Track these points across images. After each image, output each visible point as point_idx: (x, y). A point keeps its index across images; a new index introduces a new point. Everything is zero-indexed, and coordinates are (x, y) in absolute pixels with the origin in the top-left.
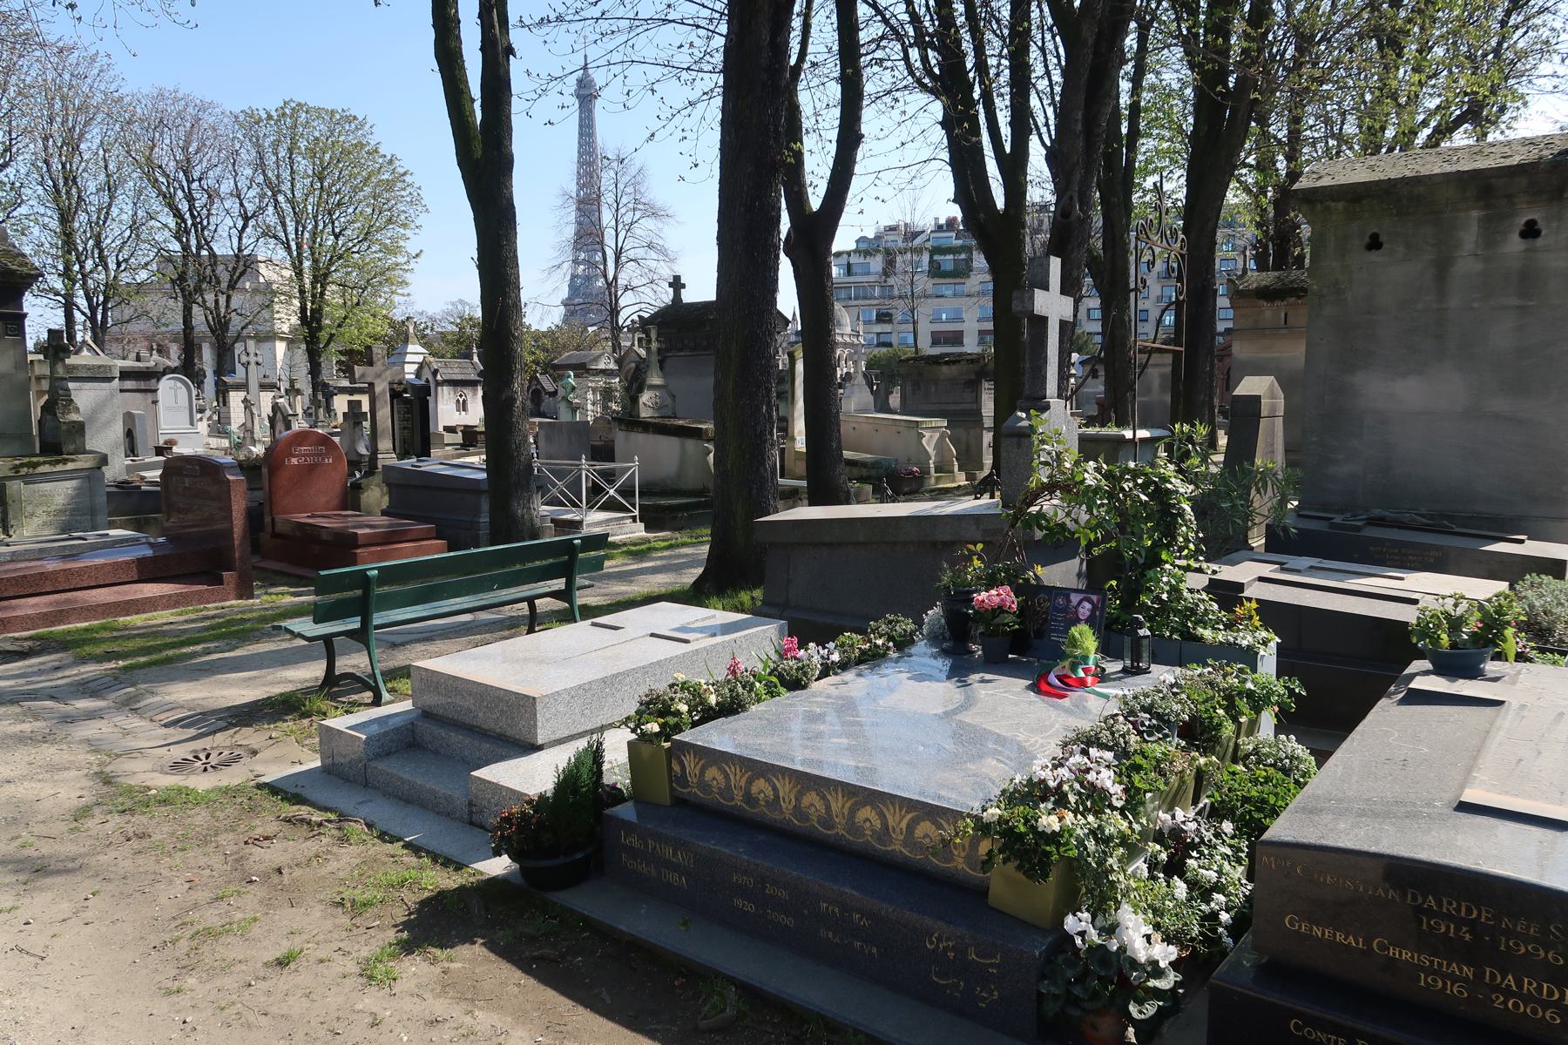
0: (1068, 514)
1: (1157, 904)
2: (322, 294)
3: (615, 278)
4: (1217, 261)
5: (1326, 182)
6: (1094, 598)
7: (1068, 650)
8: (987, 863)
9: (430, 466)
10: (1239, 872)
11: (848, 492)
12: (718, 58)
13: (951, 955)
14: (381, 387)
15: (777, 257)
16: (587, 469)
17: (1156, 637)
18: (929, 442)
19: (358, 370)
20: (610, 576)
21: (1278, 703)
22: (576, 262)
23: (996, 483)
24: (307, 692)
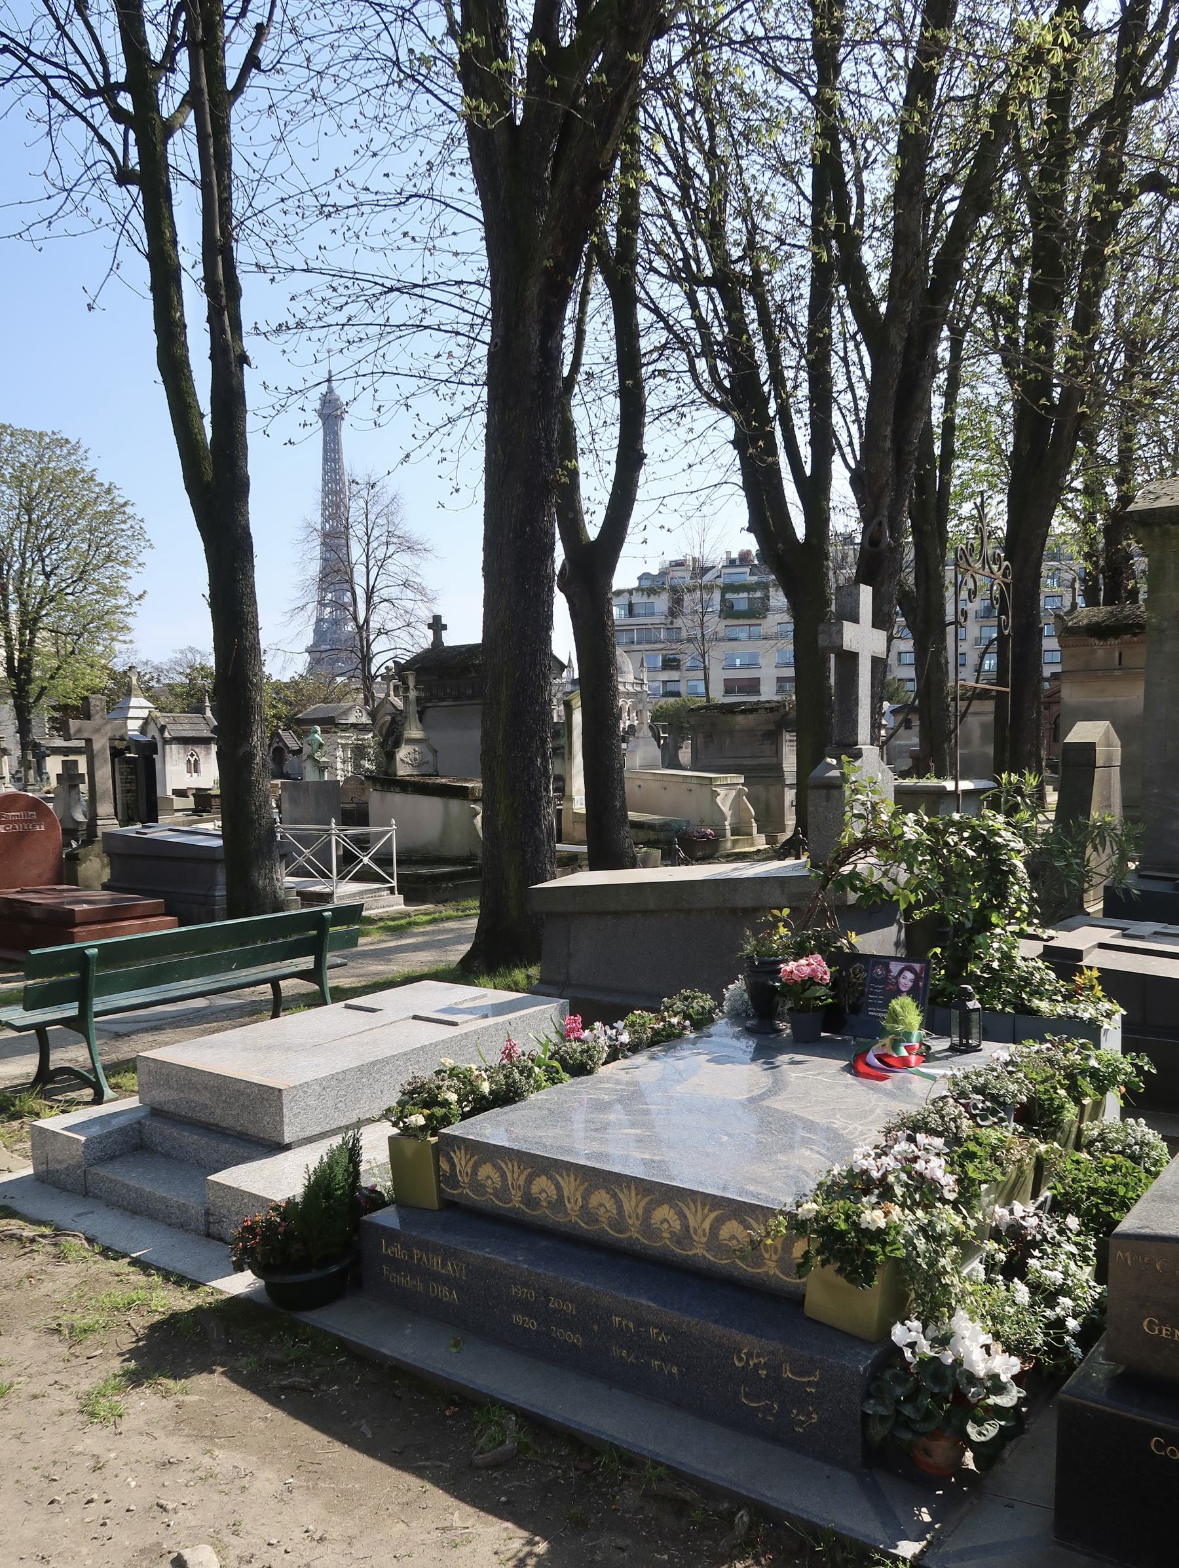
0: (885, 874)
1: (997, 1311)
2: (31, 641)
3: (367, 621)
4: (1042, 597)
5: (1164, 502)
6: (917, 967)
7: (889, 1026)
8: (804, 1266)
9: (157, 833)
10: (1086, 1273)
11: (634, 858)
12: (482, 369)
13: (763, 1373)
14: (101, 744)
15: (551, 590)
16: (337, 834)
17: (987, 1011)
18: (725, 800)
19: (74, 724)
20: (365, 955)
21: (1125, 1084)
22: (321, 603)
23: (802, 843)
24: (18, 1090)
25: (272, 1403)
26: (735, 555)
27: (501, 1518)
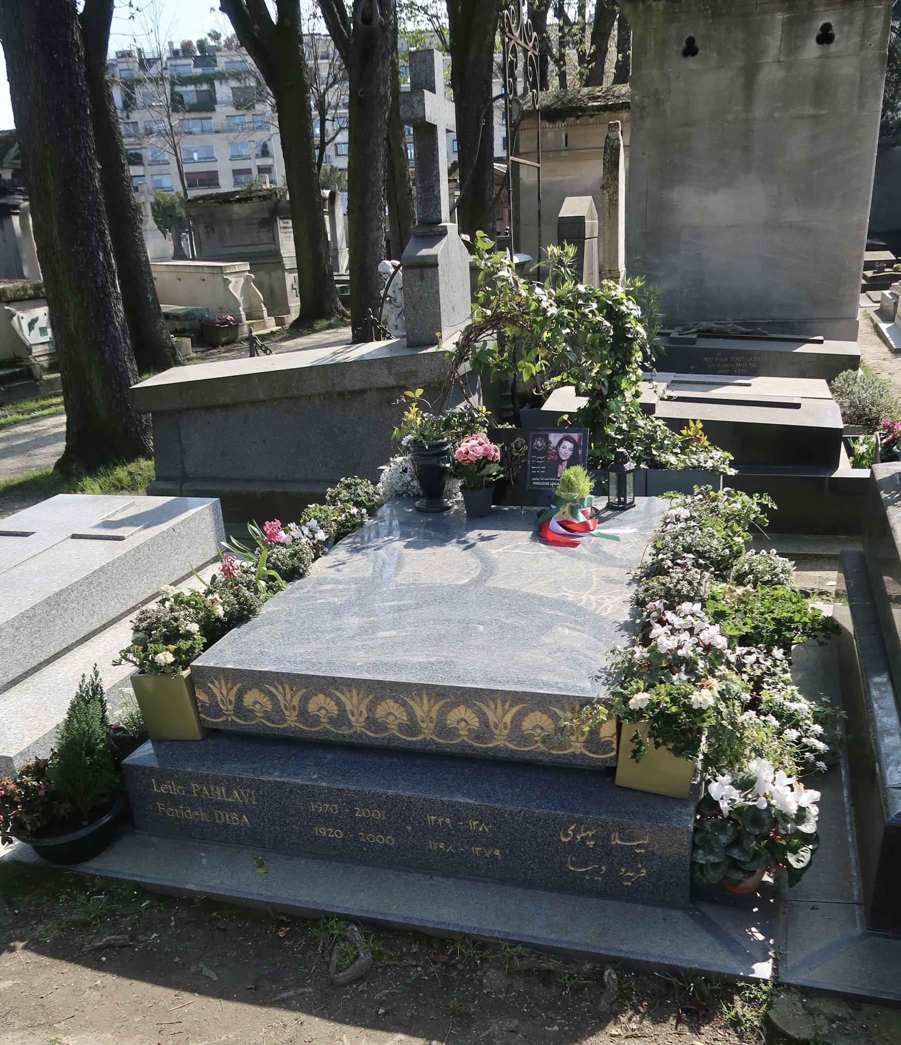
6: (575, 436)
13: (591, 844)
18: (236, 286)
25: (94, 968)
26: (177, 46)
27: (389, 1031)
